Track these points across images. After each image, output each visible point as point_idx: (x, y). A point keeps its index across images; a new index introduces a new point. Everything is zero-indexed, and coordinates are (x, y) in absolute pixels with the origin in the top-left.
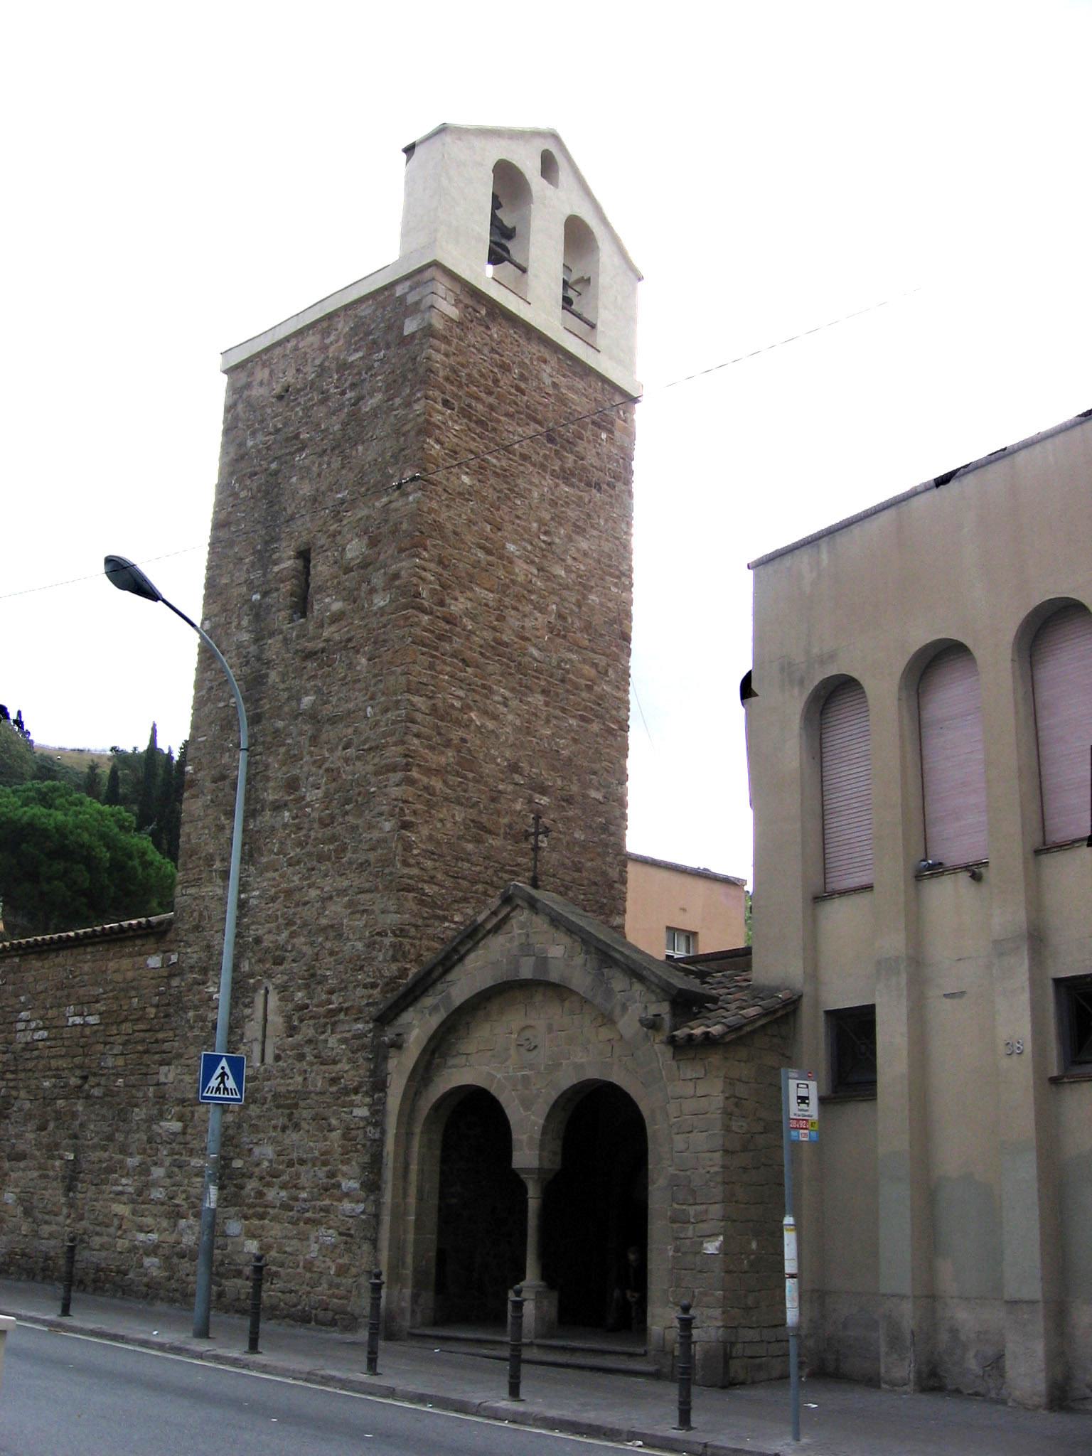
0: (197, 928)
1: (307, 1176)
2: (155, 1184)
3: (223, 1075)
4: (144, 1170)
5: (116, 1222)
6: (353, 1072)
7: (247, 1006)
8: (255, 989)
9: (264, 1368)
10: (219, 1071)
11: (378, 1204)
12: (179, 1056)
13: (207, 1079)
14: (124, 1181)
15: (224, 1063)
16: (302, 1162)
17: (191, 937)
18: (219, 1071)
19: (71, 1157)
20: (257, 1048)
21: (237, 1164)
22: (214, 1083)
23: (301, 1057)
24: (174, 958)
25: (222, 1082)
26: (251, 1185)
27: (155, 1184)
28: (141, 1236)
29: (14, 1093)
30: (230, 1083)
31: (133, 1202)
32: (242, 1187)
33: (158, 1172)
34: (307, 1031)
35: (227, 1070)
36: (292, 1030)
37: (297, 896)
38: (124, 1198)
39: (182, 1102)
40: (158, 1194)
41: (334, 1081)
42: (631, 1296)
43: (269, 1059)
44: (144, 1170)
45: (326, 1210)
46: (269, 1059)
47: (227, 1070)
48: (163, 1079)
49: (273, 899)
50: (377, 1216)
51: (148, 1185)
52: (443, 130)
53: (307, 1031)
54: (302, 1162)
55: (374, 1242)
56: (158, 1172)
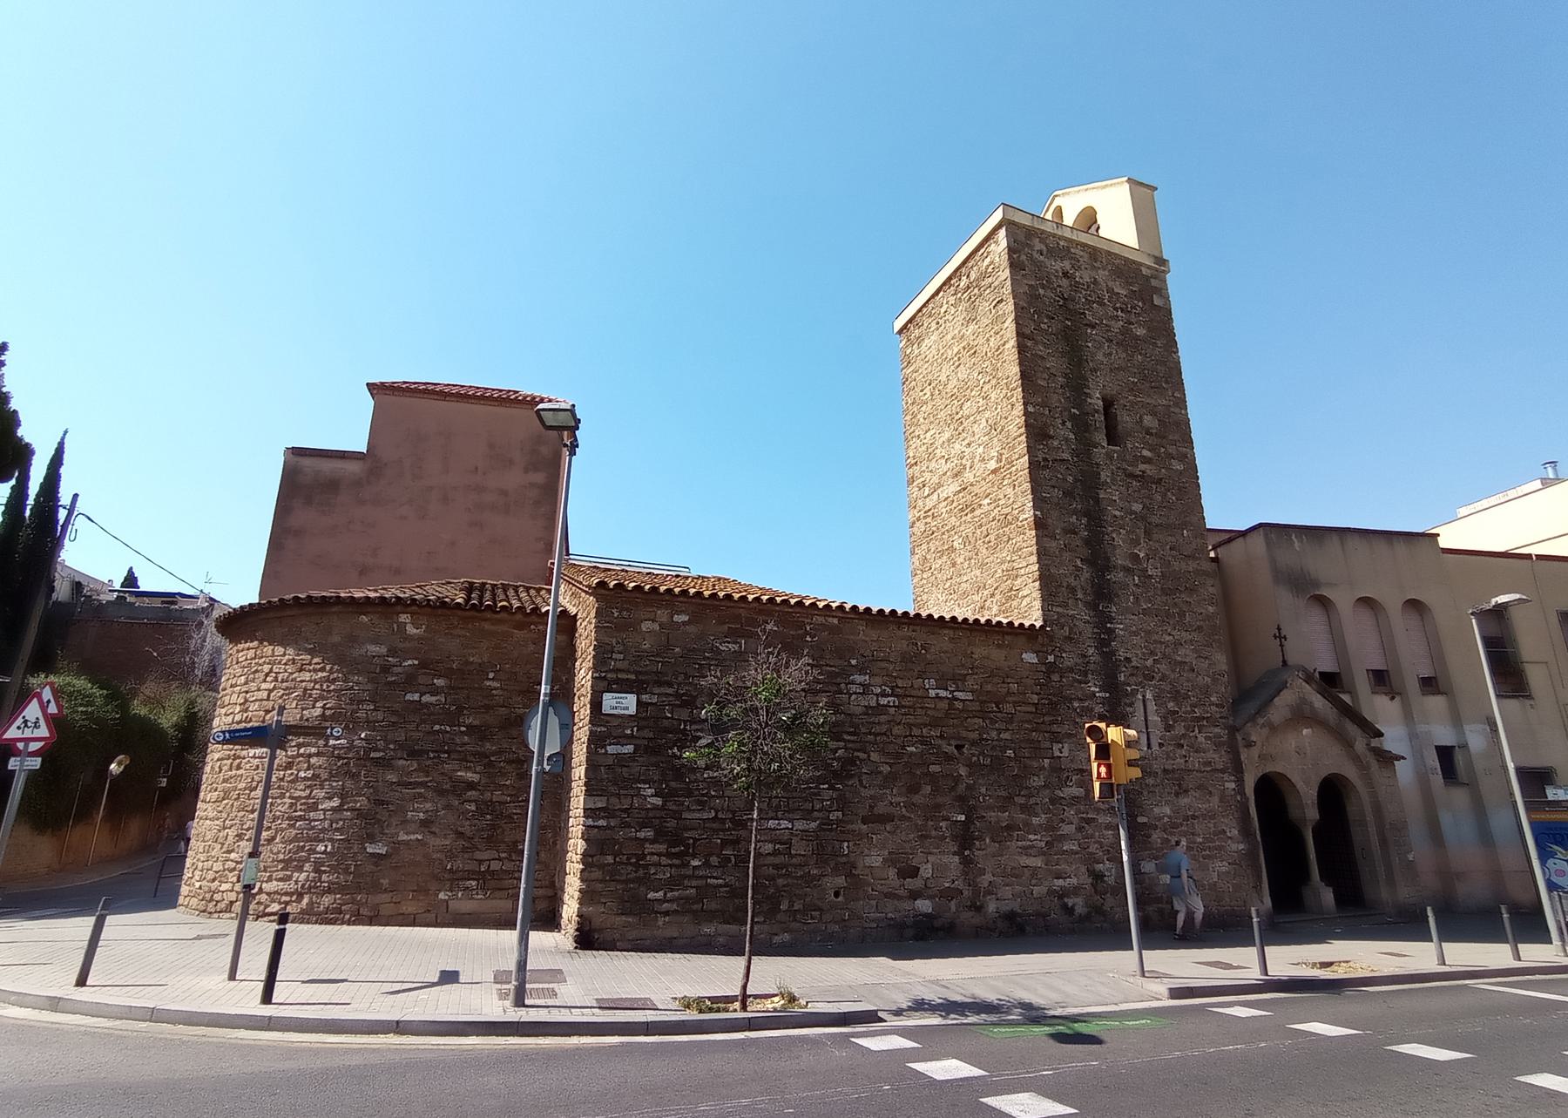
2: (1064, 837)
6: (1219, 759)
7: (1131, 705)
14: (1032, 837)
16: (1194, 817)
19: (963, 818)
24: (1051, 659)
27: (1064, 837)
31: (1044, 854)
33: (1068, 829)
34: (1179, 729)
36: (1168, 728)
42: (1031, 409)
44: (1050, 827)
45: (1220, 848)
46: (1155, 747)
48: (1057, 754)
49: (1136, 634)
52: (1260, 525)
53: (1179, 729)
54: (1194, 817)
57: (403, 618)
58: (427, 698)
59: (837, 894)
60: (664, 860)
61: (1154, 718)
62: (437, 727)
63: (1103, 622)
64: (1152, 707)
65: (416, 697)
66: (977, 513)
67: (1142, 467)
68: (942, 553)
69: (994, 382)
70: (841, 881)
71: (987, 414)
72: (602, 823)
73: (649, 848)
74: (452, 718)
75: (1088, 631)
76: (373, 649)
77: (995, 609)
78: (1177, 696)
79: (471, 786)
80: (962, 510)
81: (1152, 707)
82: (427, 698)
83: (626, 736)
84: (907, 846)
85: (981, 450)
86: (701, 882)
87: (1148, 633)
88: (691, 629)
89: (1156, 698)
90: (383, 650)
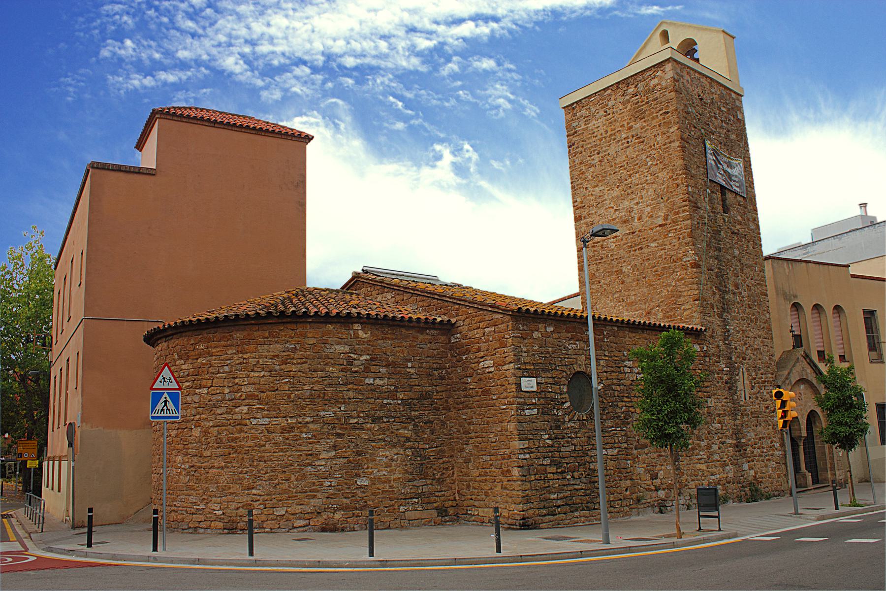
0: (712, 336)
1: (766, 443)
3: (166, 402)
4: (709, 447)
5: (700, 473)
8: (738, 368)
9: (99, 555)
10: (163, 399)
11: (785, 451)
12: (715, 394)
13: (154, 405)
14: (701, 453)
15: (166, 395)
16: (763, 438)
17: (711, 340)
18: (163, 399)
20: (743, 392)
21: (743, 441)
22: (160, 406)
23: (757, 398)
24: (705, 348)
25: (166, 405)
26: (749, 449)
28: (713, 477)
29: (632, 410)
30: (171, 406)
31: (706, 462)
32: (745, 450)
35: (168, 399)
36: (752, 388)
37: (746, 333)
38: (702, 461)
39: (719, 415)
40: (716, 457)
41: (767, 408)
43: (747, 398)
46: (747, 398)
47: (168, 399)
50: (785, 455)
51: (712, 454)
54: (763, 438)
55: (785, 464)
56: (715, 447)
57: (357, 326)
58: (378, 382)
59: (626, 490)
60: (556, 476)
61: (746, 382)
62: (385, 401)
63: (725, 323)
64: (745, 374)
65: (371, 381)
66: (645, 250)
67: (738, 227)
68: (611, 273)
69: (661, 166)
70: (628, 483)
71: (655, 186)
72: (528, 456)
73: (549, 469)
74: (392, 395)
75: (719, 331)
76: (340, 348)
77: (660, 315)
78: (756, 369)
79: (408, 440)
80: (631, 247)
81: (745, 374)
82: (378, 382)
83: (533, 404)
84: (654, 461)
85: (649, 209)
86: (572, 488)
87: (744, 331)
88: (555, 335)
89: (748, 370)
90: (347, 349)
